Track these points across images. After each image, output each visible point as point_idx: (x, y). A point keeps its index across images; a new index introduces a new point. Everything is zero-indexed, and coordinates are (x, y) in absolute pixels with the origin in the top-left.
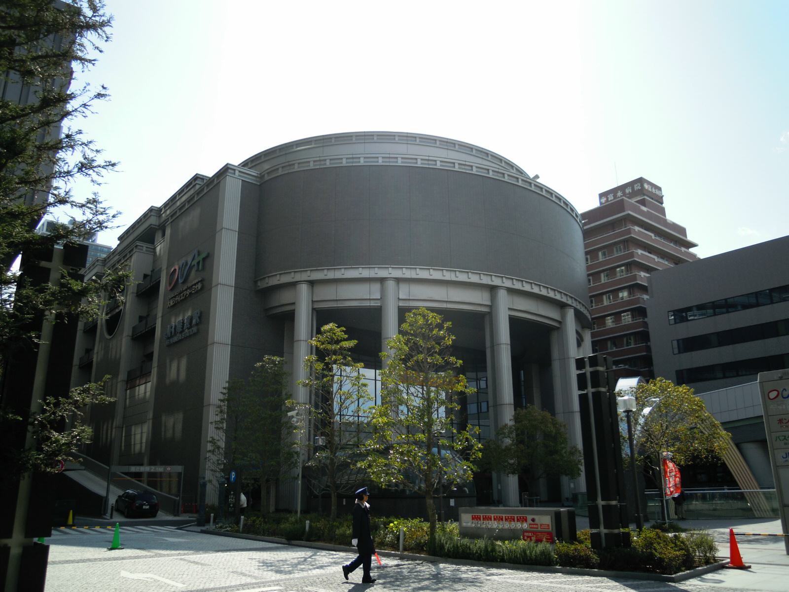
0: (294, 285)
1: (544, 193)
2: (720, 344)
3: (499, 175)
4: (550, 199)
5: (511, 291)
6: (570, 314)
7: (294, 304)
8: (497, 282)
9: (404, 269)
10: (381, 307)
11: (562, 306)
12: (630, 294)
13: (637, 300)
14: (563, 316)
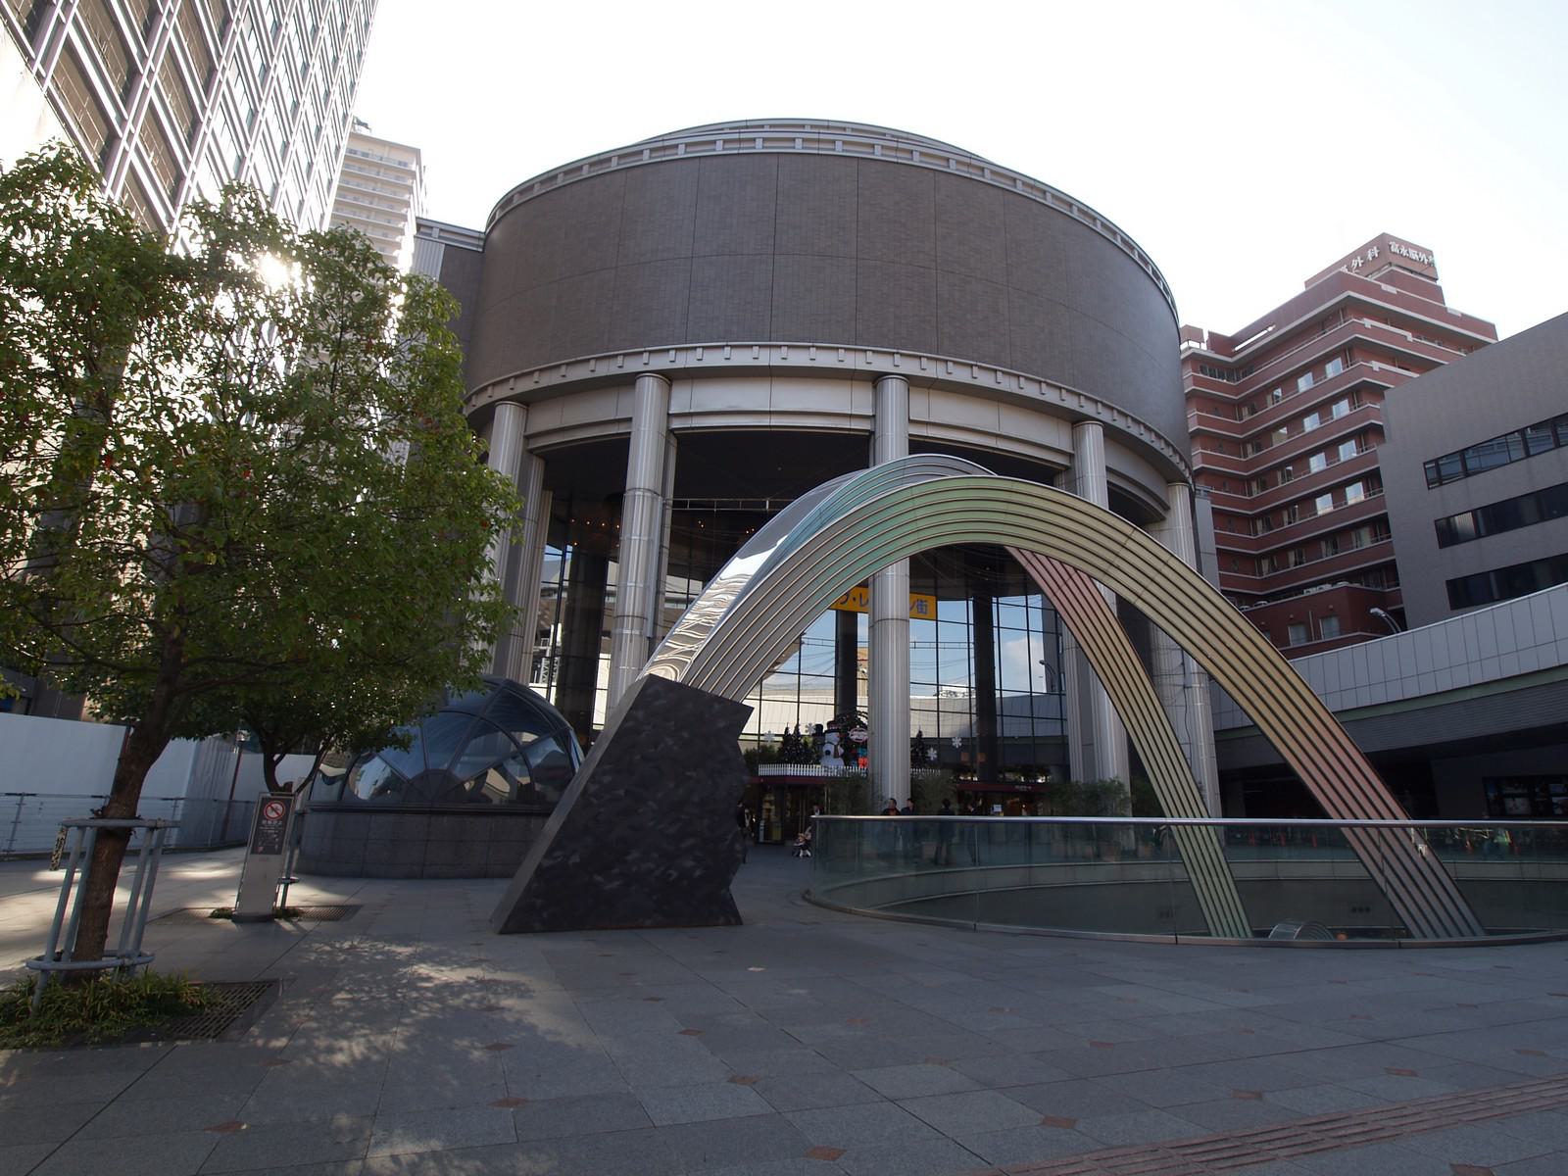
0: (629, 381)
1: (1075, 214)
2: (1544, 516)
3: (1035, 193)
4: (1092, 229)
5: (912, 382)
6: (1093, 436)
7: (630, 420)
8: (880, 364)
9: (869, 354)
10: (872, 433)
11: (1076, 421)
12: (1352, 404)
13: (1367, 413)
14: (1077, 441)
